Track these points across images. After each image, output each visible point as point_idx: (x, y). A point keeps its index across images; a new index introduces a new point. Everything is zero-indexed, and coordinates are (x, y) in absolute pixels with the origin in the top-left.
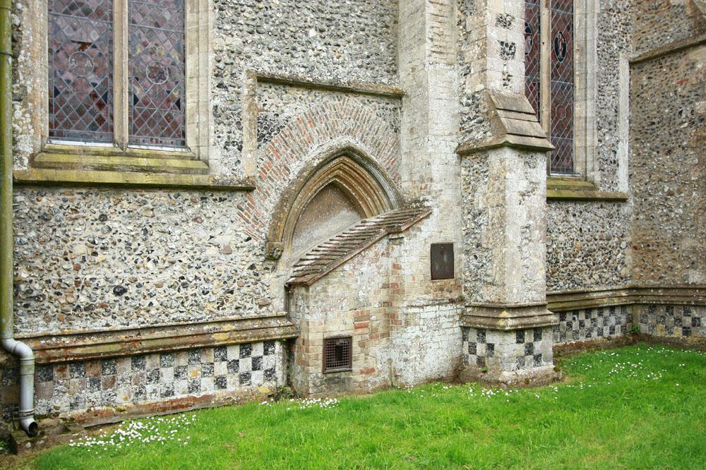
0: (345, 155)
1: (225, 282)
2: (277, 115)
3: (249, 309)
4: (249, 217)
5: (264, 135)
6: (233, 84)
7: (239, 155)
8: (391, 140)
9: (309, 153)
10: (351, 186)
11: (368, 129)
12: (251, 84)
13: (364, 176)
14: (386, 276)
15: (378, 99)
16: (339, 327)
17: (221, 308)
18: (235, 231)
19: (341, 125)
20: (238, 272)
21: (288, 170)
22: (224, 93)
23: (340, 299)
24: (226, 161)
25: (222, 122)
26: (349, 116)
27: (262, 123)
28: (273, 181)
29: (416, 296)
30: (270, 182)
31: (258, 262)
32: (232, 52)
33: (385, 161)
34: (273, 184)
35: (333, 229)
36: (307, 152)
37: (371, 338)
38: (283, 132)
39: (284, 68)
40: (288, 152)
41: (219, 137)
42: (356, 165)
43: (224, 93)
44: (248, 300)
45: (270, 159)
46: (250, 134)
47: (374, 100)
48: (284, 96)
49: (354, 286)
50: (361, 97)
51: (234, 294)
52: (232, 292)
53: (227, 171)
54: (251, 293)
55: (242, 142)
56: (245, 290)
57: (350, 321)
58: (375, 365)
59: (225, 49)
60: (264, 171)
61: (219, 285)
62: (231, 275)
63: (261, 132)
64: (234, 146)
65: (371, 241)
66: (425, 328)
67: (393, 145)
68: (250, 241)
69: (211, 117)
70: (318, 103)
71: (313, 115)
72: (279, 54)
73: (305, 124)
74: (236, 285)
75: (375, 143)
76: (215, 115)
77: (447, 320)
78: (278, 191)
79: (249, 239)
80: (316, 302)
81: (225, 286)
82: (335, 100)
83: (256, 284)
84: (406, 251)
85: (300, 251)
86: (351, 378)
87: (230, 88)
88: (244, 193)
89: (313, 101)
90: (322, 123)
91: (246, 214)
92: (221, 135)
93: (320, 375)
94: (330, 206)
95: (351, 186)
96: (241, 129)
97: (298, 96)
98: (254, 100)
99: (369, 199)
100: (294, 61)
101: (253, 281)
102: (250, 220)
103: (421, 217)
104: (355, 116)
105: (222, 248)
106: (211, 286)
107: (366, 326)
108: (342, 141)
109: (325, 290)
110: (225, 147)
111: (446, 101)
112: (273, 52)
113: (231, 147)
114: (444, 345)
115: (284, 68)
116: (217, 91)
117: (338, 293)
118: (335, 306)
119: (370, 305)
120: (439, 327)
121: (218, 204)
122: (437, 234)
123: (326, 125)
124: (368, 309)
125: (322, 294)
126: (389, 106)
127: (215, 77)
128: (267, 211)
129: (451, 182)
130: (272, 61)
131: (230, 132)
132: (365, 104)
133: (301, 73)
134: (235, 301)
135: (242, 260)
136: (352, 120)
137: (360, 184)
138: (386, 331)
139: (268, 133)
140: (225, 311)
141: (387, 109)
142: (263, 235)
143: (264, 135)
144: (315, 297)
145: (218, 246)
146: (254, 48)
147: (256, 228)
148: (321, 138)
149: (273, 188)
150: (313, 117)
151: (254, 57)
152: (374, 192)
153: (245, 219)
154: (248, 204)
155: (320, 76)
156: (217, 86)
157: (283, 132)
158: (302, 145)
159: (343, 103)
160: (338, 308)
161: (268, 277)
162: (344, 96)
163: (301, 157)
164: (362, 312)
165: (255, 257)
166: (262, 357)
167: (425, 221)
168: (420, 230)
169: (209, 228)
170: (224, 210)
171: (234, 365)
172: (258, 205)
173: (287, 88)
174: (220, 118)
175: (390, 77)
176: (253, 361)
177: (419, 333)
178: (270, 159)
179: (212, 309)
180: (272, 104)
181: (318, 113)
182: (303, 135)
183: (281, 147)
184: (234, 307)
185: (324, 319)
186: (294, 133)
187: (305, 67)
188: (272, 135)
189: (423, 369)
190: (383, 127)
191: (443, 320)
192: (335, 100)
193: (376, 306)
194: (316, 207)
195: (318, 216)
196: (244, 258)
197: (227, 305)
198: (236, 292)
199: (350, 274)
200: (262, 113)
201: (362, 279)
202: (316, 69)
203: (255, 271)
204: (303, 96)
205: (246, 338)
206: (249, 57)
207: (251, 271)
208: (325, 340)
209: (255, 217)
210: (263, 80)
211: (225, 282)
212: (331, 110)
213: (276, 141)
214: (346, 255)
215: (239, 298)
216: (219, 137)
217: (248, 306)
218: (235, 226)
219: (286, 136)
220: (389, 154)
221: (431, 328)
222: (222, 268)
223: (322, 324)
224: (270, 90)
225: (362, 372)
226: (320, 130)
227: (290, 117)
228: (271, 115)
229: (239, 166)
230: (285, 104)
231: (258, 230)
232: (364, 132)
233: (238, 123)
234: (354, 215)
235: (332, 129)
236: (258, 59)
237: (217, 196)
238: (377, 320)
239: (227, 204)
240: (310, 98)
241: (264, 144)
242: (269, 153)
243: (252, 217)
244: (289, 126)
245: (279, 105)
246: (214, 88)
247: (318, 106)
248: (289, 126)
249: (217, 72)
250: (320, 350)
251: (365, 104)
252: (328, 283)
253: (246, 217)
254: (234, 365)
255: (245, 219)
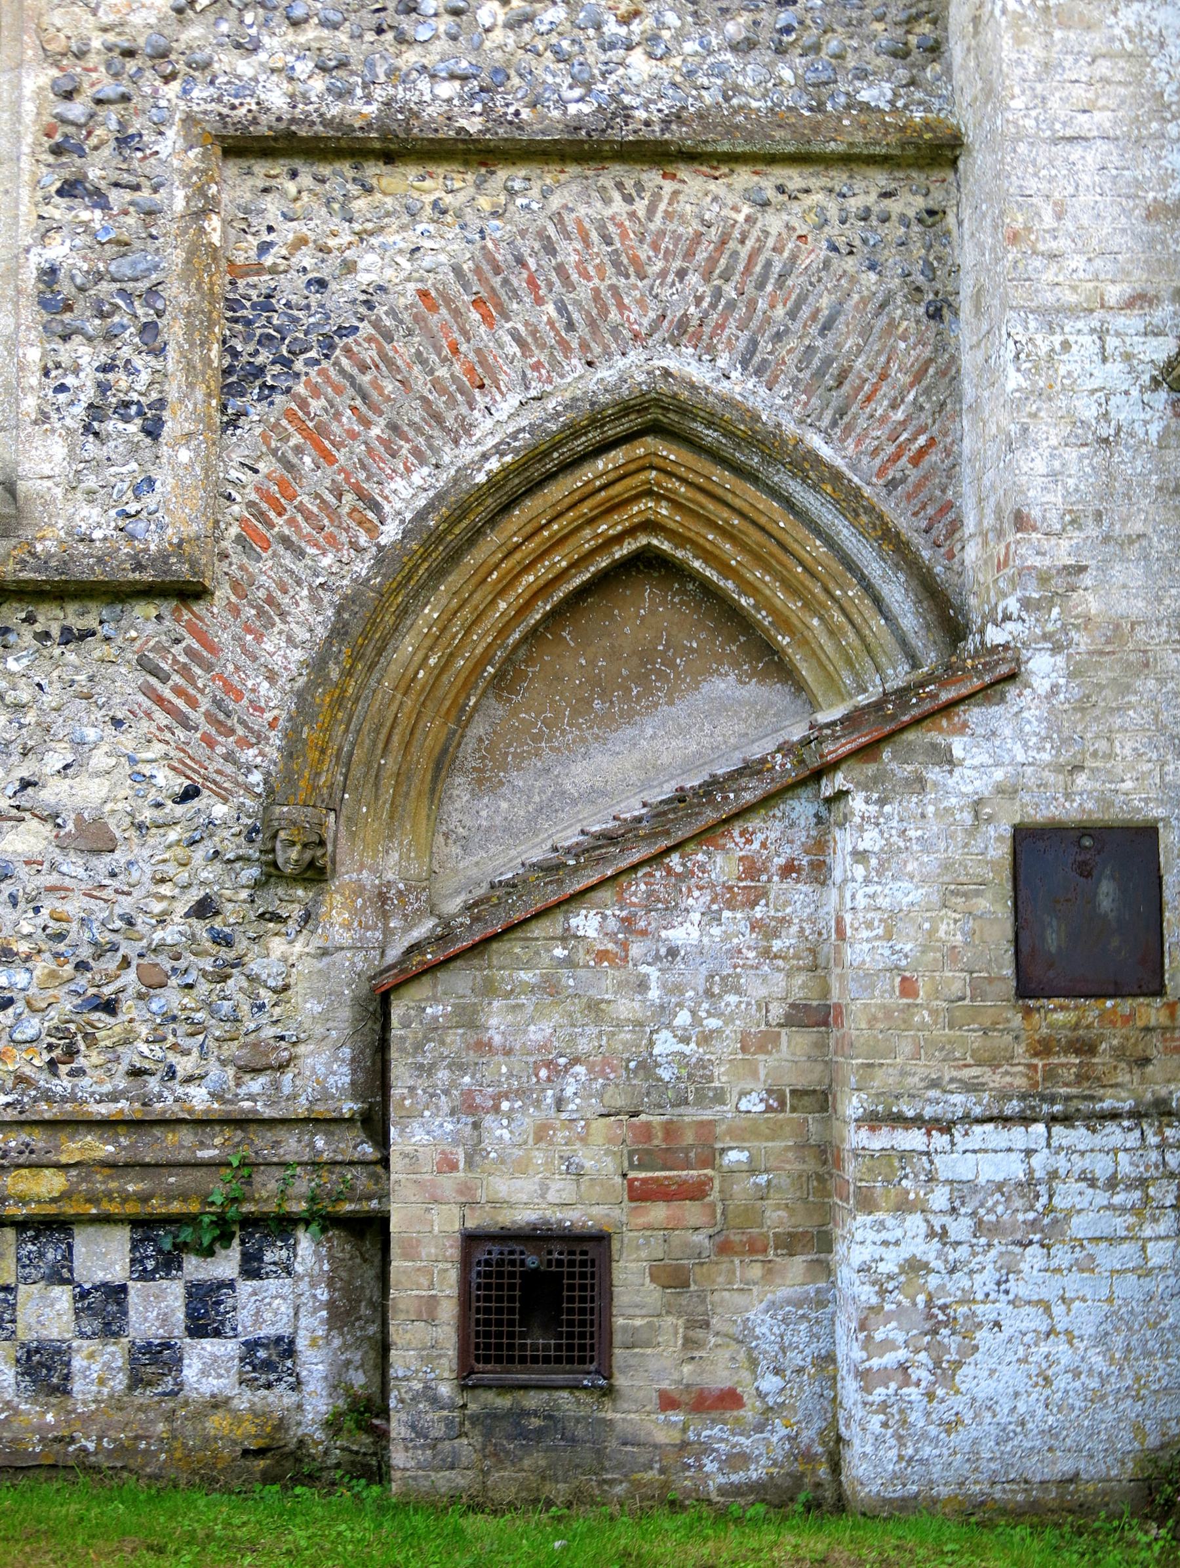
0: (656, 429)
1: (82, 966)
2: (322, 284)
3: (189, 1080)
4: (193, 703)
5: (261, 370)
6: (126, 178)
7: (148, 454)
8: (909, 353)
9: (478, 433)
10: (725, 569)
11: (780, 312)
12: (195, 170)
13: (763, 520)
14: (814, 968)
15: (838, 178)
16: (544, 1189)
17: (63, 1069)
18: (133, 761)
19: (641, 303)
20: (140, 927)
21: (376, 507)
22: (85, 215)
23: (548, 1064)
24: (91, 482)
25: (79, 331)
26: (677, 264)
27: (248, 323)
28: (300, 554)
29: (923, 1069)
30: (288, 560)
31: (235, 894)
32: (129, 53)
33: (875, 452)
34: (297, 567)
35: (665, 759)
36: (467, 428)
37: (725, 1248)
38: (348, 351)
39: (359, 92)
40: (375, 431)
41: (62, 388)
42: (720, 476)
43: (85, 215)
44: (185, 1043)
45: (289, 466)
46: (190, 367)
47: (813, 183)
48: (360, 205)
49: (626, 1007)
50: (744, 177)
51: (123, 1017)
52: (110, 1007)
53: (96, 520)
54: (199, 1016)
55: (161, 403)
56: (171, 999)
57: (600, 1160)
58: (745, 1375)
59: (96, 44)
60: (261, 516)
61: (53, 975)
62: (105, 937)
63: (245, 358)
64: (126, 419)
65: (717, 807)
66: (960, 1228)
67: (919, 377)
68: (195, 803)
69: (30, 313)
70: (522, 219)
71: (497, 270)
72: (343, 37)
73: (456, 313)
74: (130, 977)
75: (819, 374)
76: (44, 304)
77: (1102, 1198)
78: (326, 597)
79: (189, 794)
80: (427, 1070)
81: (83, 980)
82: (607, 201)
83: (225, 978)
84: (860, 856)
85: (493, 849)
86: (610, 1423)
87: (114, 195)
88: (167, 607)
89: (495, 214)
90: (539, 301)
91: (178, 691)
92: (70, 381)
93: (445, 1390)
94: (646, 656)
95: (725, 569)
96: (159, 352)
97: (428, 199)
98: (202, 231)
99: (815, 622)
100: (411, 57)
101: (207, 964)
102: (197, 717)
103: (945, 696)
104: (712, 261)
105: (70, 827)
106: (21, 978)
107: (696, 1192)
108: (625, 370)
109: (468, 1018)
110: (87, 429)
111: (1103, 146)
112: (311, 34)
113: (112, 425)
114: (1085, 1319)
115: (359, 92)
116: (58, 210)
117: (536, 1033)
118: (520, 1093)
119: (719, 1097)
120: (1048, 1229)
121: (57, 651)
122: (1050, 777)
123: (562, 308)
124: (707, 1115)
125: (455, 1038)
126: (895, 206)
127: (51, 159)
128: (272, 677)
129: (1137, 527)
130: (303, 68)
131: (105, 369)
132: (766, 204)
133: (438, 100)
134: (126, 1042)
135: (157, 884)
136: (693, 279)
137: (759, 559)
138: (805, 1223)
139: (280, 360)
140: (85, 1081)
141: (885, 219)
142: (256, 777)
143: (261, 370)
144: (418, 1047)
145: (52, 818)
146: (224, 27)
147: (220, 750)
148: (537, 367)
149: (299, 583)
150: (497, 281)
151: (226, 61)
152: (827, 590)
153: (171, 710)
154: (188, 651)
155: (533, 105)
156: (60, 192)
157: (348, 351)
158: (440, 402)
159: (651, 210)
160: (538, 1103)
161: (280, 952)
162: (652, 177)
163: (436, 451)
164: (670, 1130)
165: (218, 866)
166: (231, 1285)
167: (974, 714)
168: (947, 760)
169: (16, 748)
170: (81, 678)
171: (104, 1307)
172: (231, 654)
173: (373, 170)
174: (67, 317)
175: (902, 74)
176: (190, 1294)
177: (928, 1251)
178: (289, 466)
179: (28, 1071)
180: (302, 242)
181: (521, 262)
182: (444, 360)
183: (338, 416)
184: (124, 1067)
185: (493, 1151)
186: (402, 351)
187: (464, 78)
188: (299, 365)
189: (950, 1427)
190: (864, 301)
191: (1068, 1195)
192: (607, 201)
193: (753, 1104)
194: (576, 657)
195: (589, 702)
196: (171, 869)
197: (88, 1059)
198: (129, 1008)
199: (603, 955)
200: (253, 280)
201: (687, 978)
202: (516, 81)
203: (217, 923)
204: (448, 199)
205: (144, 1198)
206: (206, 65)
207: (200, 927)
208: (471, 1240)
209: (218, 703)
210: (243, 145)
211: (82, 966)
212: (587, 244)
213: (316, 392)
214: (576, 869)
215: (144, 1031)
216: (62, 388)
217: (185, 1065)
218: (127, 741)
219: (364, 368)
220: (899, 415)
221: (996, 1229)
222: (73, 907)
223: (454, 1167)
224: (291, 187)
225: (668, 1402)
226: (534, 333)
227: (381, 288)
228: (290, 288)
229: (151, 501)
230: (360, 236)
231: (229, 757)
232: (761, 329)
233: (148, 329)
234: (775, 694)
235: (592, 324)
236: (246, 67)
237: (51, 618)
238: (753, 1171)
239: (97, 654)
240: (484, 203)
241: (262, 407)
242: (287, 439)
243: (205, 704)
244: (377, 324)
245: (332, 243)
246: (47, 200)
247: (523, 233)
248: (377, 324)
249: (58, 138)
250: (446, 1285)
251: (766, 204)
252: (489, 989)
253: (180, 703)
254: (104, 1307)
255: (171, 710)
